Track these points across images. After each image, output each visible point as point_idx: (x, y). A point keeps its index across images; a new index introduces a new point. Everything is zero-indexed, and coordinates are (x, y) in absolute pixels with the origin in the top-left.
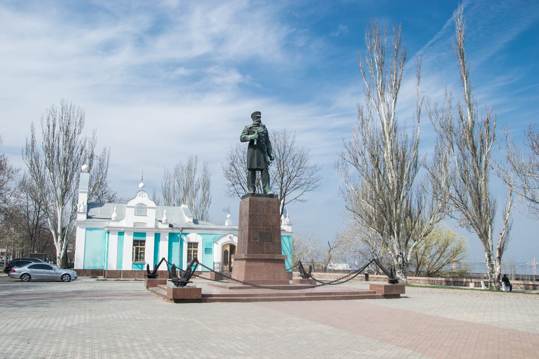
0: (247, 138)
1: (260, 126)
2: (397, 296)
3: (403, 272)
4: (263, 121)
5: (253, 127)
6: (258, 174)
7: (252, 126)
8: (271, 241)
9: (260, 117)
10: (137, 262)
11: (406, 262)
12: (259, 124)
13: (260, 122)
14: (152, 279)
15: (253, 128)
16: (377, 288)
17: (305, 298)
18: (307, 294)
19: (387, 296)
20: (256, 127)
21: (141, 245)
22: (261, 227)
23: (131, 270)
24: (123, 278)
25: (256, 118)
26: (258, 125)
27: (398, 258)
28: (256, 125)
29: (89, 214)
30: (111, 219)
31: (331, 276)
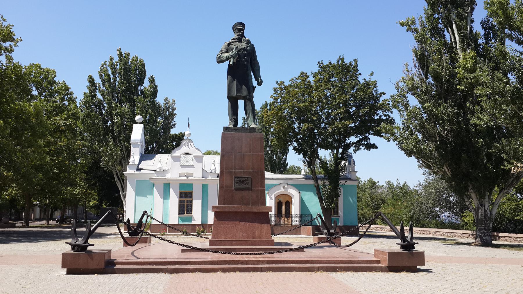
0: (223, 57)
1: (243, 41)
2: (413, 269)
3: (485, 228)
4: (248, 34)
5: (233, 42)
6: (241, 103)
7: (231, 41)
8: (252, 190)
9: (243, 30)
10: (287, 199)
11: (489, 215)
12: (241, 38)
13: (242, 36)
14: (135, 236)
15: (232, 44)
16: (381, 256)
17: (262, 268)
18: (269, 262)
19: (393, 268)
20: (236, 43)
21: (188, 197)
22: (237, 171)
23: (177, 223)
24: (169, 233)
25: (237, 31)
26: (239, 40)
27: (478, 211)
28: (236, 40)
29: (140, 167)
30: (156, 170)
31: (417, 231)
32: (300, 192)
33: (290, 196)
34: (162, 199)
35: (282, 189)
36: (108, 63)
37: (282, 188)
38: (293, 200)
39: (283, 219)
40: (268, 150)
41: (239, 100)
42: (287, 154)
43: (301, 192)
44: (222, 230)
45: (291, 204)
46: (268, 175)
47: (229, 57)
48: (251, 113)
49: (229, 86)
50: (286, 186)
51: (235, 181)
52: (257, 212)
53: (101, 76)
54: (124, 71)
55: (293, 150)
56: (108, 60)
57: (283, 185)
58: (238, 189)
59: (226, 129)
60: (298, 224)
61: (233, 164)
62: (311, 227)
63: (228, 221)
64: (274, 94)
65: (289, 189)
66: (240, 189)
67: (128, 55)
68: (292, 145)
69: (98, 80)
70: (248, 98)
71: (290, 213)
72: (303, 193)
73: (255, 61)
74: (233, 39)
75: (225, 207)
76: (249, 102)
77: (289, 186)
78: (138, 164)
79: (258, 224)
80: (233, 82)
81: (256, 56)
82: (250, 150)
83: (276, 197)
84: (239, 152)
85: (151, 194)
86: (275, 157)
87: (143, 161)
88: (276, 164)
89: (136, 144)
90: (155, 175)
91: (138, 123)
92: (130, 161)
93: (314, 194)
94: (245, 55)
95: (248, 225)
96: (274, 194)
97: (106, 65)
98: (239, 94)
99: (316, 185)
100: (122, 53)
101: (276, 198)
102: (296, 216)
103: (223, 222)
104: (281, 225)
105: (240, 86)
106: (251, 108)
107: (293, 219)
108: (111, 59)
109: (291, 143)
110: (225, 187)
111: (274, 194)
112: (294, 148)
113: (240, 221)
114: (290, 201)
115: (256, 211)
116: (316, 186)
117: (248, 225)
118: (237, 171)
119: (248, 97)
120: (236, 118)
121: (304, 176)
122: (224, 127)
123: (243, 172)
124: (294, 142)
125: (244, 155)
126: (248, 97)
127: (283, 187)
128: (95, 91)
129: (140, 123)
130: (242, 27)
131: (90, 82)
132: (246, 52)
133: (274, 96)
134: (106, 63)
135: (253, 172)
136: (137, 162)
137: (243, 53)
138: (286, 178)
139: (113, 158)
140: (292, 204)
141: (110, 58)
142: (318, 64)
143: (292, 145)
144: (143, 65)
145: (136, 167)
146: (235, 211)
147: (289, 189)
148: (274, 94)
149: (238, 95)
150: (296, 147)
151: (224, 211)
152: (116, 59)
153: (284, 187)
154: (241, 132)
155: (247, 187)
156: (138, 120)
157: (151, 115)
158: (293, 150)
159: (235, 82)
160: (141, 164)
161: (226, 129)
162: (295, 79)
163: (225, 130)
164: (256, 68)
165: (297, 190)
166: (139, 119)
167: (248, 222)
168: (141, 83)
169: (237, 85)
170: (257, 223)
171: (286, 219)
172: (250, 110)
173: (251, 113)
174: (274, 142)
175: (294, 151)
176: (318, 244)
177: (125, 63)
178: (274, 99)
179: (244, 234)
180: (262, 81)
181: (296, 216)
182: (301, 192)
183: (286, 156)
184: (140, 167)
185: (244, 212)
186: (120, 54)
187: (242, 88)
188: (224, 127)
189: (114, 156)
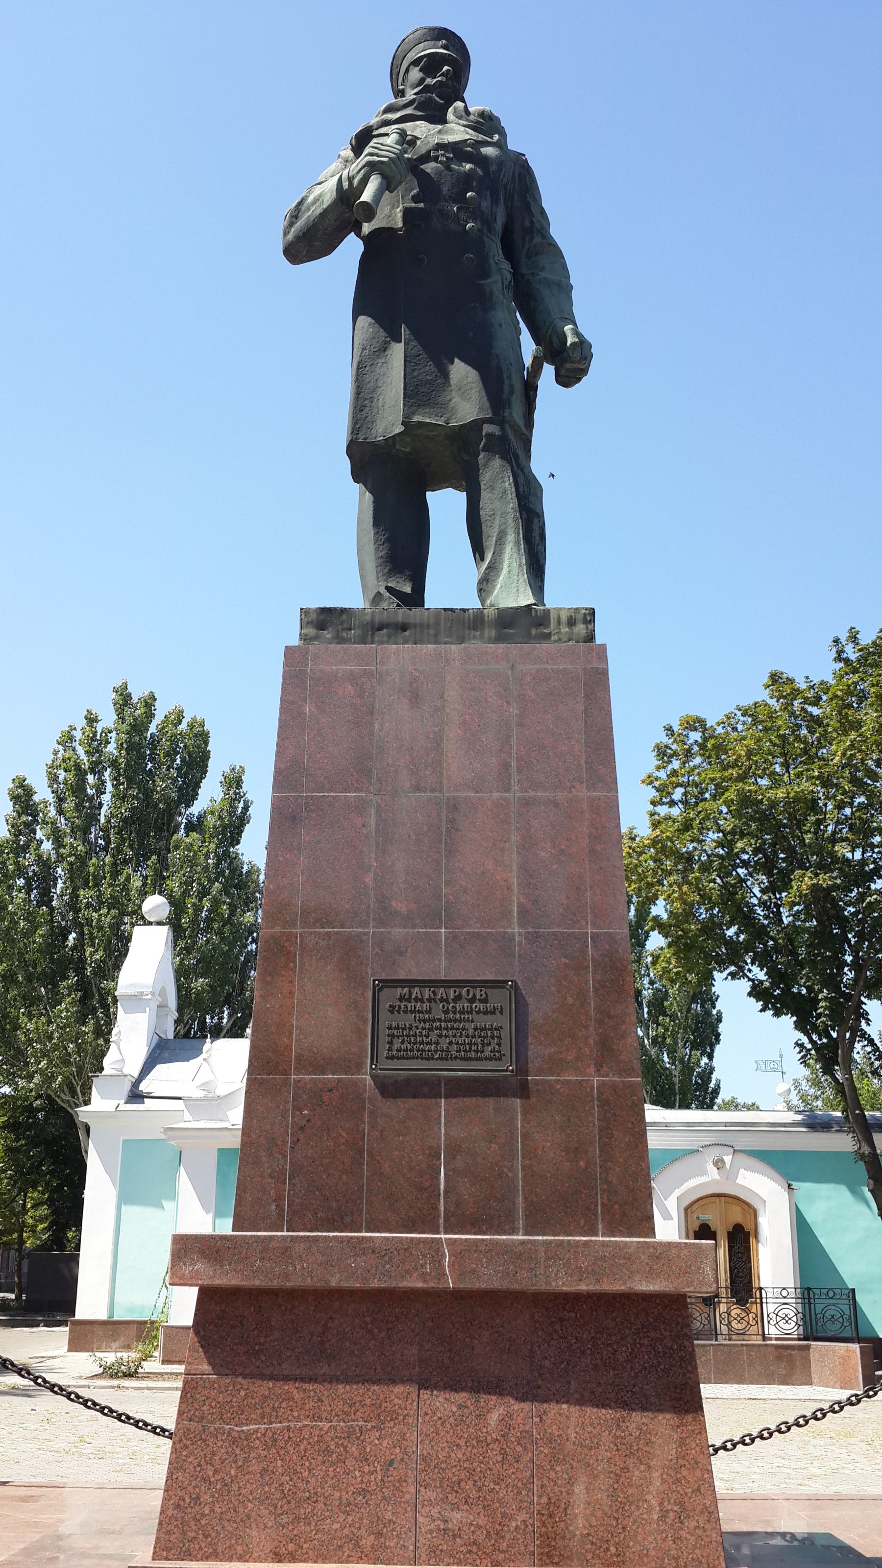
7: (374, 121)
8: (523, 1090)
10: (736, 1216)
29: (143, 1087)
32: (789, 1185)
33: (749, 1205)
34: (211, 1215)
35: (713, 1173)
36: (78, 735)
37: (711, 1168)
38: (762, 1220)
39: (723, 1307)
40: (640, 1033)
41: (429, 494)
42: (712, 1051)
43: (795, 1185)
44: (255, 1467)
45: (752, 1240)
46: (653, 1113)
47: (356, 182)
48: (511, 537)
49: (357, 380)
50: (728, 1159)
51: (384, 1015)
52: (577, 1298)
53: (53, 779)
54: (128, 754)
55: (750, 994)
56: (81, 722)
57: (715, 1152)
58: (408, 1081)
59: (321, 626)
60: (791, 1328)
61: (369, 879)
62: (856, 1347)
63: (312, 1380)
64: (658, 768)
65: (742, 1171)
66: (426, 1081)
67: (149, 703)
68: (745, 975)
69: (43, 793)
70: (489, 436)
71: (750, 1282)
72: (803, 1188)
73: (537, 239)
74: (389, 109)
75: (286, 1249)
76: (497, 462)
77: (741, 1157)
78: (136, 1075)
79: (591, 1412)
80: (384, 348)
81: (543, 212)
82: (506, 766)
83: (686, 1209)
84: (417, 788)
85: (173, 1196)
86: (666, 1059)
87: (159, 1067)
88: (673, 1084)
89: (137, 1000)
90: (187, 1116)
91: (150, 923)
92: (106, 1062)
93: (854, 1191)
94: (467, 180)
95: (494, 1418)
96: (678, 1193)
97: (71, 739)
98: (423, 415)
99: (866, 1149)
100: (129, 696)
101: (688, 1210)
102: (784, 1293)
103: (264, 1387)
104: (716, 1335)
105: (431, 367)
106: (512, 504)
107: (770, 1308)
108: (91, 720)
109: (741, 969)
110: (303, 1064)
111: (678, 1193)
112: (754, 987)
113: (424, 1384)
114: (749, 1227)
115: (564, 1283)
116: (862, 1157)
117: (494, 1418)
118: (398, 932)
119: (487, 428)
120: (408, 589)
121: (799, 1117)
122: (304, 612)
123: (452, 938)
124: (753, 963)
125: (454, 806)
126: (487, 428)
127: (716, 1163)
128: (30, 828)
129: (159, 923)
130: (444, 47)
131: (15, 798)
132: (468, 166)
133: (657, 779)
134: (74, 733)
135: (533, 938)
136: (134, 1069)
137: (448, 168)
138: (726, 1124)
139: (67, 1063)
140: (758, 1241)
141: (86, 718)
142: (834, 650)
143: (745, 975)
144: (204, 737)
145: (127, 1086)
146: (375, 1284)
147: (742, 1171)
148: (658, 768)
149: (416, 418)
150: (761, 982)
151: (275, 1283)
152: (108, 718)
153: (719, 1164)
154: (436, 642)
155: (486, 1069)
156: (150, 911)
157: (216, 903)
158: (750, 994)
159: (397, 351)
160: (149, 1077)
161: (321, 626)
162: (739, 713)
163: (311, 631)
164: (543, 275)
165: (779, 1177)
166: (158, 907)
167: (497, 1388)
168: (189, 794)
169: (407, 361)
170: (581, 1402)
171: (736, 1311)
172: (504, 514)
173: (511, 537)
174: (664, 964)
175: (753, 1000)
176: (856, 1395)
177: (138, 727)
178: (658, 790)
179: (456, 1517)
180: (583, 350)
181: (784, 1293)
182: (795, 1185)
183: (711, 1057)
184: (143, 1087)
185: (459, 1296)
186: (123, 699)
187: (446, 375)
188: (304, 612)
189: (69, 1055)
